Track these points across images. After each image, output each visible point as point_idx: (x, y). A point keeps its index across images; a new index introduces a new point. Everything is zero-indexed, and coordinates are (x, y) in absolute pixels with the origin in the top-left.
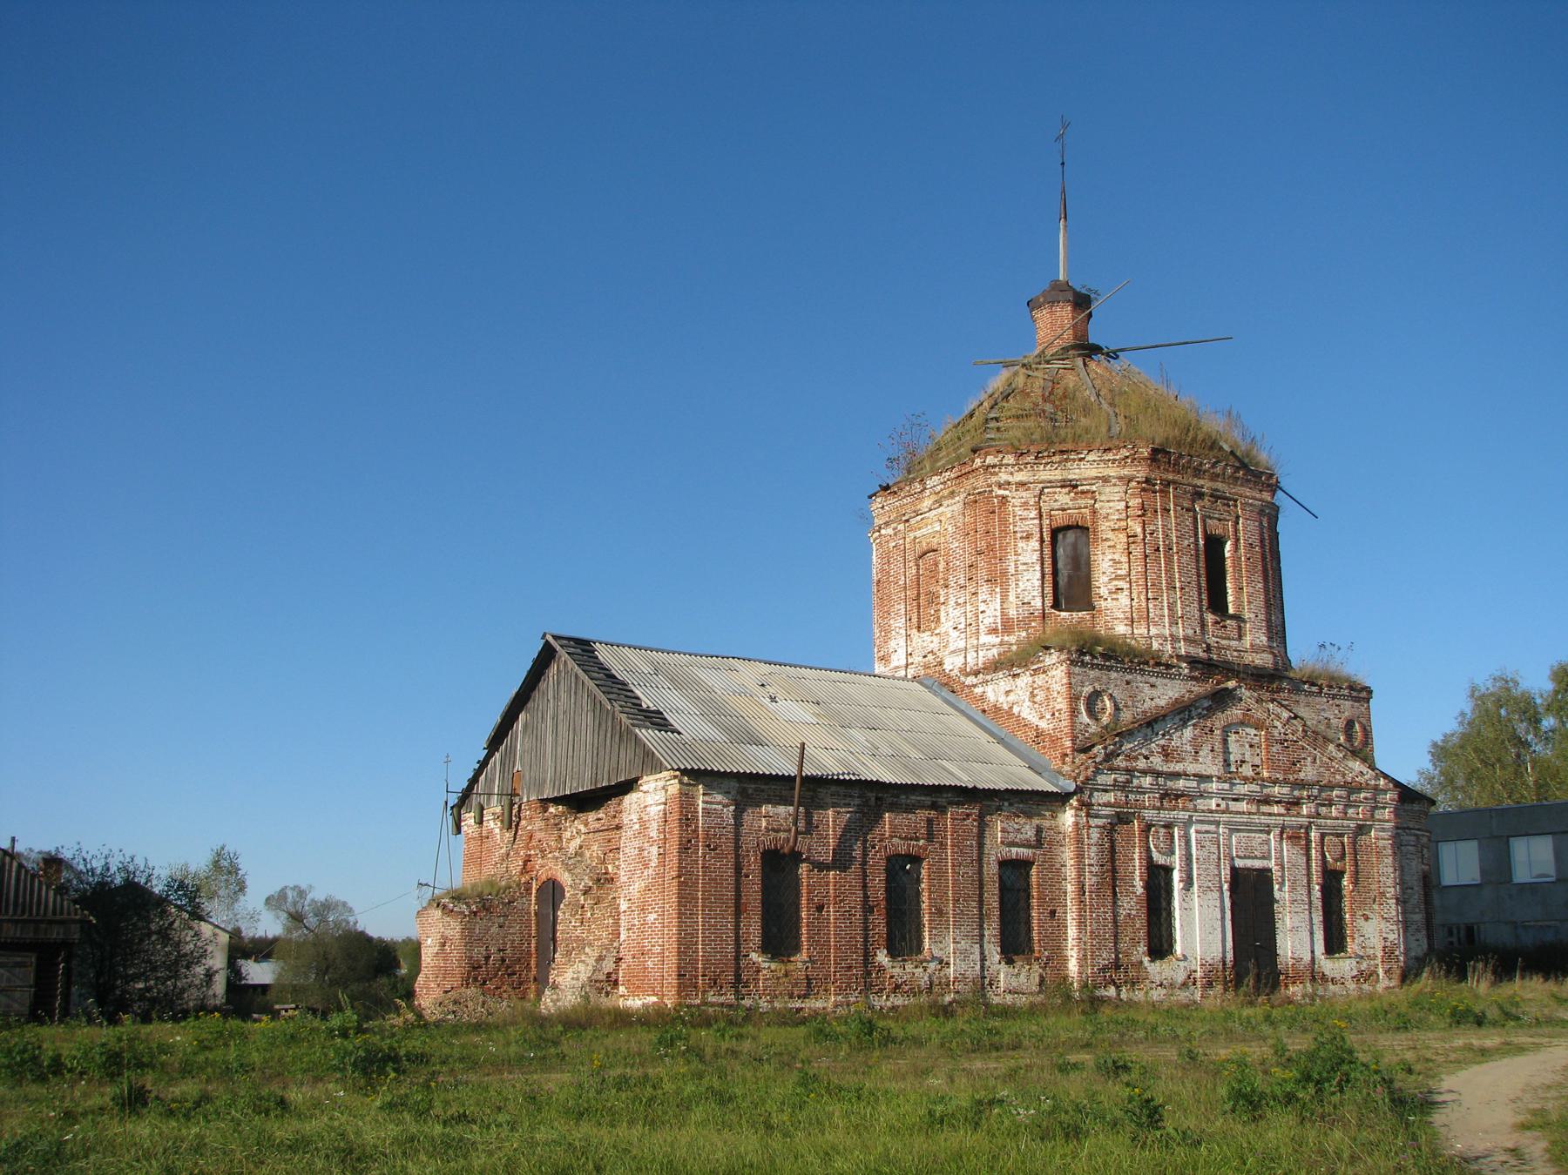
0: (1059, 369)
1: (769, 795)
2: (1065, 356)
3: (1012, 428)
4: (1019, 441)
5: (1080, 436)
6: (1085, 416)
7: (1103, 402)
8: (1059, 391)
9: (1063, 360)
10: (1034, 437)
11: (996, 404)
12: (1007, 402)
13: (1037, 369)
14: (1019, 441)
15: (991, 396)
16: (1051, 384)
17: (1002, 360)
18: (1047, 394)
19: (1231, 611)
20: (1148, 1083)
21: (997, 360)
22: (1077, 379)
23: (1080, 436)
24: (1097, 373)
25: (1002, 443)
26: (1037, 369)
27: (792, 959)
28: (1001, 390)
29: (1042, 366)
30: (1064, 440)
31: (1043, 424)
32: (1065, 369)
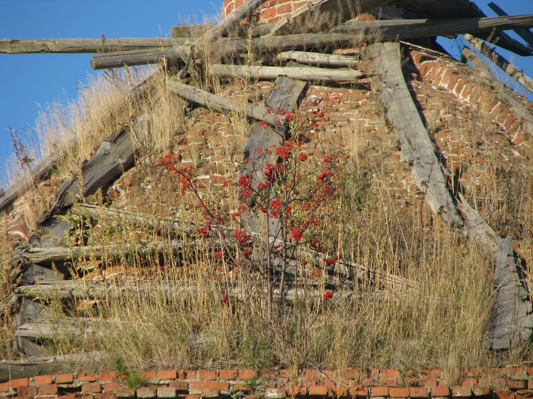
0: (310, 82)
1: (322, 229)
2: (334, 37)
3: (123, 302)
4: (147, 353)
5: (379, 343)
6: (402, 268)
7: (472, 215)
8: (304, 168)
9: (328, 48)
10: (202, 338)
11: (64, 209)
12: (107, 201)
13: (225, 81)
14: (147, 353)
15: (45, 176)
16: (276, 139)
17: (96, 42)
18: (260, 177)
19: (308, 9)
20: (385, 163)
21: (72, 41)
22: (379, 124)
23: (379, 343)
24: (454, 107)
25: (80, 357)
26: (225, 81)
27: (441, 40)
28: (85, 154)
29: (244, 70)
30: (320, 358)
31: (239, 292)
32: (332, 83)
